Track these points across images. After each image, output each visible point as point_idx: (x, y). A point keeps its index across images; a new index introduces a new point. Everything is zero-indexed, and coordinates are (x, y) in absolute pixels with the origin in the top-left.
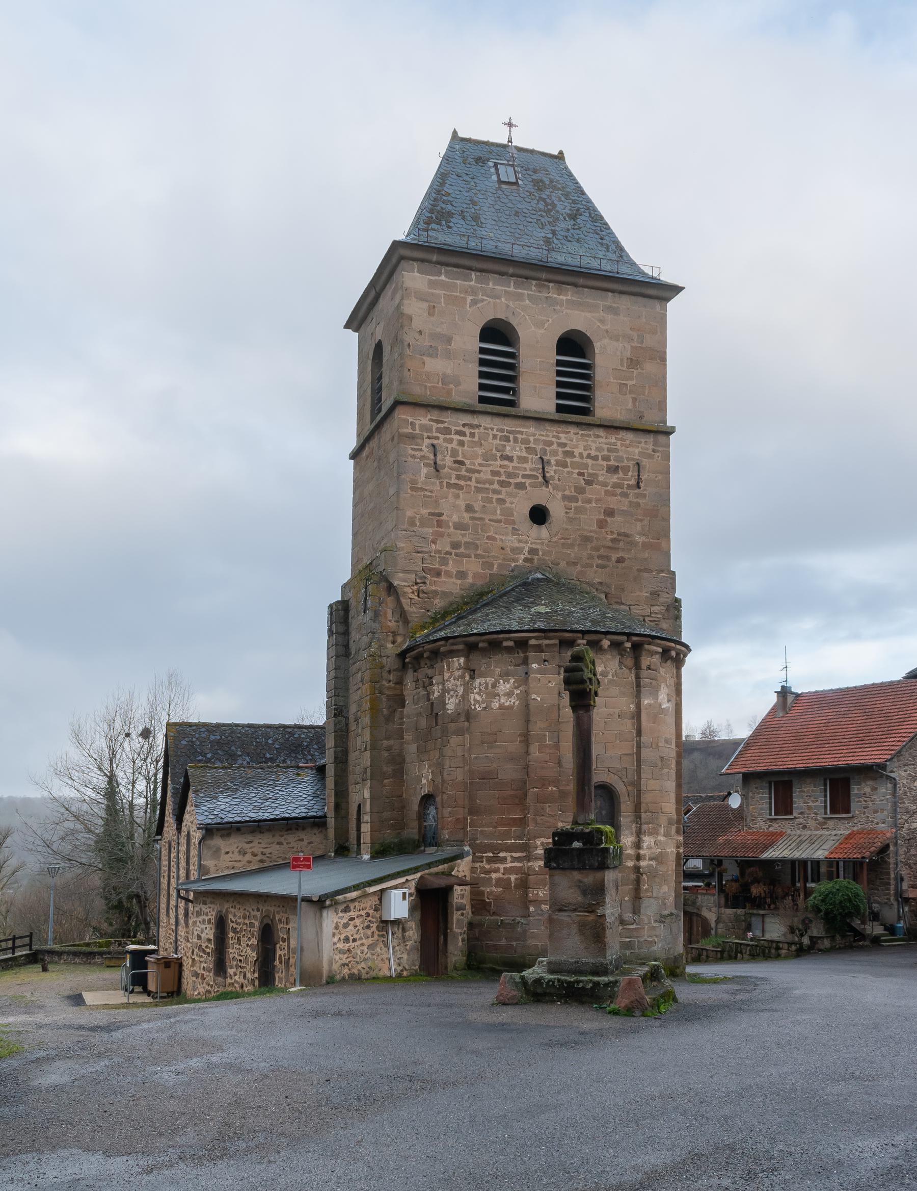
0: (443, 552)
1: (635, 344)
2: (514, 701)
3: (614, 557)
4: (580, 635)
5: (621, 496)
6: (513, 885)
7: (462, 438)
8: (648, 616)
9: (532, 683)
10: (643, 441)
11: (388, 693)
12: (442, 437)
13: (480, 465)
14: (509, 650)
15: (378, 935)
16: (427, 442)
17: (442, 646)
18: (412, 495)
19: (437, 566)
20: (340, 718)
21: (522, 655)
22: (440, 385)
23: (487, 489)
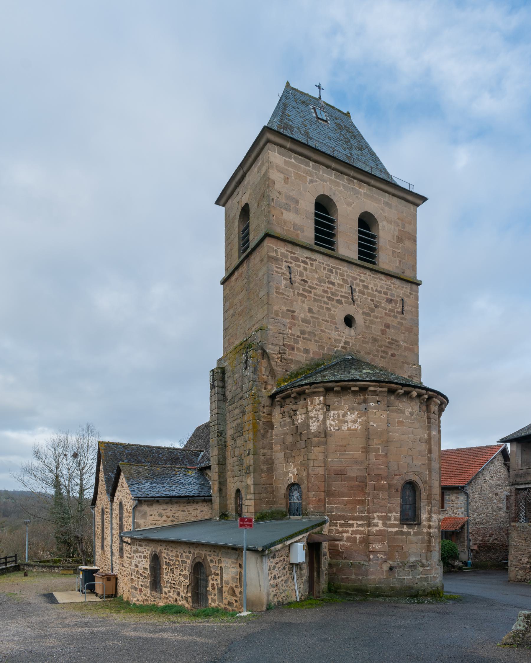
1: (400, 228)
2: (357, 426)
4: (400, 387)
5: (394, 317)
6: (358, 541)
7: (305, 266)
10: (405, 287)
11: (263, 420)
12: (294, 263)
13: (317, 285)
14: (354, 392)
16: (285, 264)
17: (307, 389)
18: (277, 297)
19: (292, 344)
20: (221, 438)
21: (362, 397)
22: (292, 229)
23: (321, 300)
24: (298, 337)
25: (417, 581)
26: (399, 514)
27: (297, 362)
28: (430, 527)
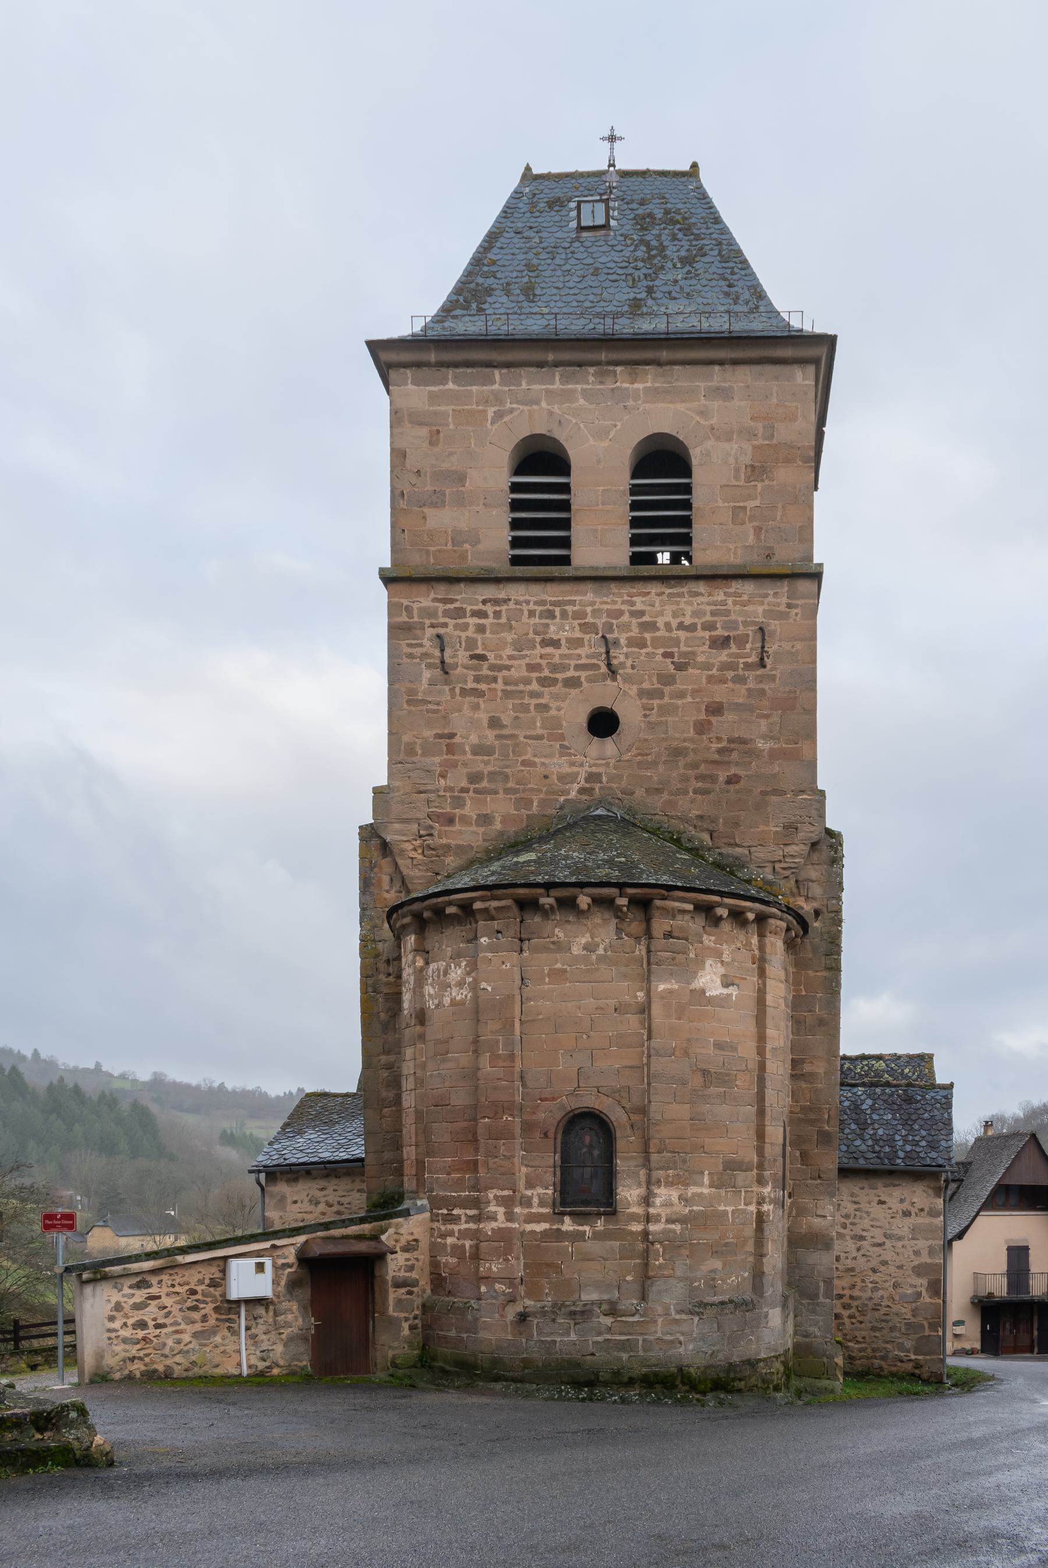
0: (456, 789)
1: (760, 441)
3: (722, 776)
4: (541, 891)
6: (468, 1254)
8: (780, 861)
9: (482, 966)
10: (771, 592)
11: (385, 991)
12: (451, 622)
13: (511, 657)
15: (217, 1319)
18: (410, 712)
19: (448, 810)
22: (450, 546)
23: (521, 692)
24: (465, 790)
25: (591, 1349)
26: (550, 1192)
27: (461, 849)
28: (648, 1219)
